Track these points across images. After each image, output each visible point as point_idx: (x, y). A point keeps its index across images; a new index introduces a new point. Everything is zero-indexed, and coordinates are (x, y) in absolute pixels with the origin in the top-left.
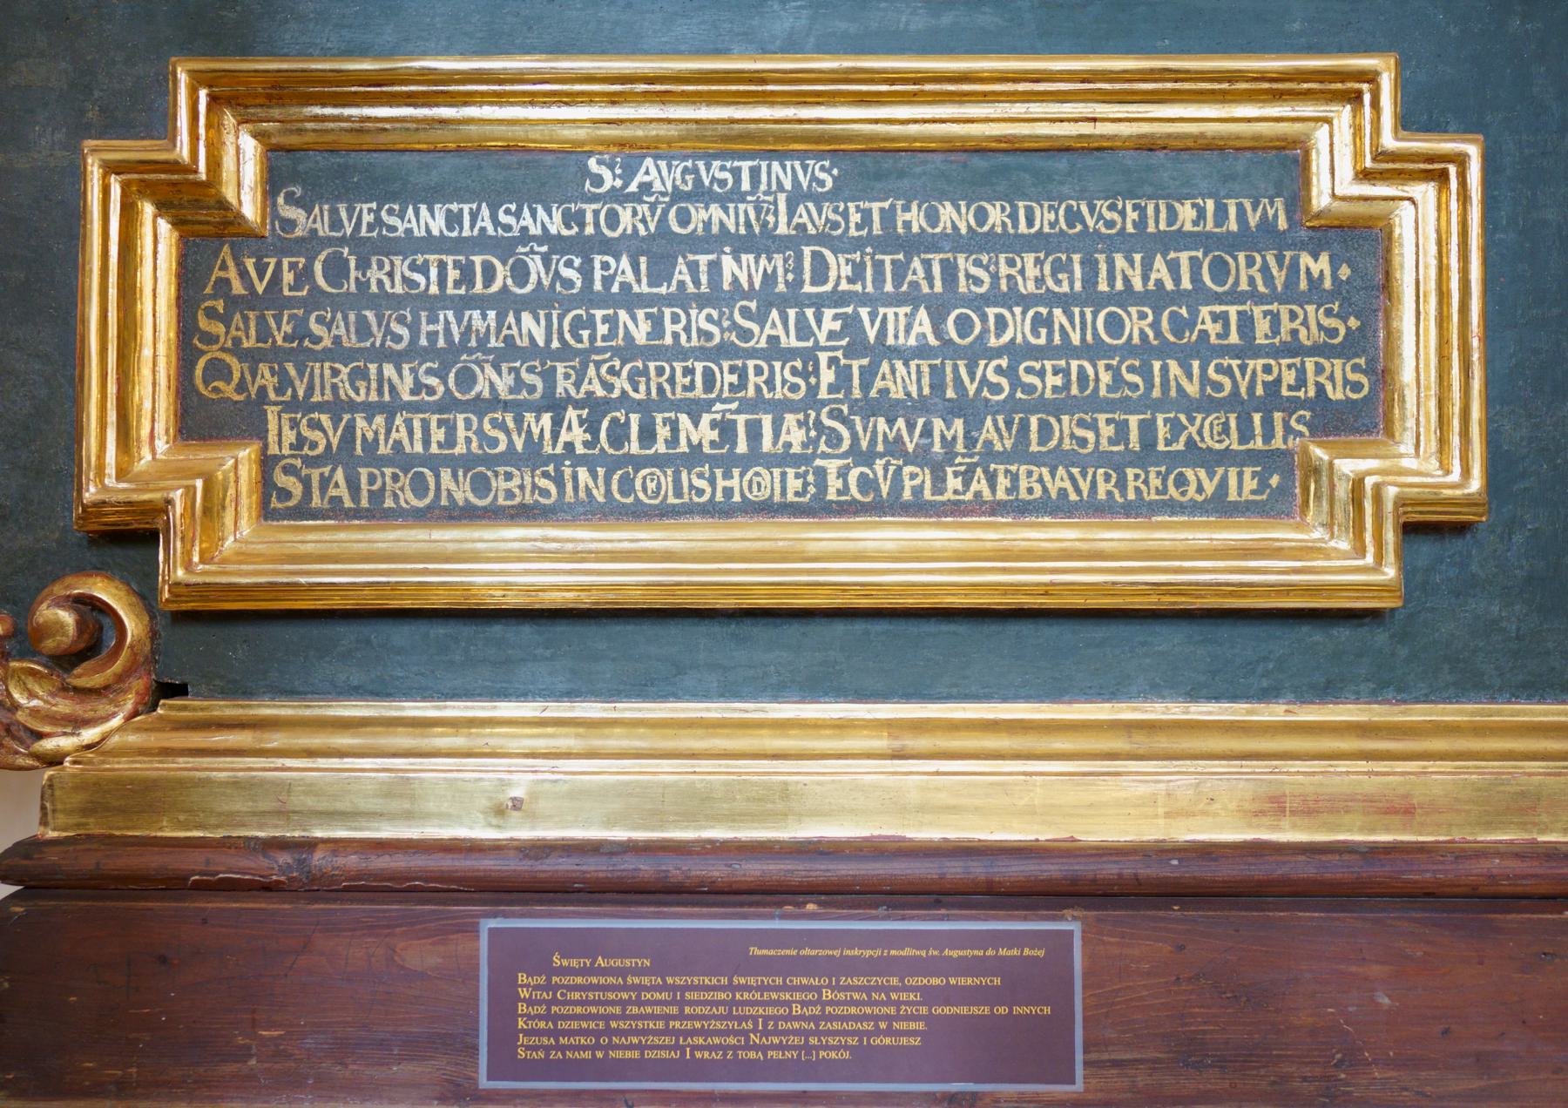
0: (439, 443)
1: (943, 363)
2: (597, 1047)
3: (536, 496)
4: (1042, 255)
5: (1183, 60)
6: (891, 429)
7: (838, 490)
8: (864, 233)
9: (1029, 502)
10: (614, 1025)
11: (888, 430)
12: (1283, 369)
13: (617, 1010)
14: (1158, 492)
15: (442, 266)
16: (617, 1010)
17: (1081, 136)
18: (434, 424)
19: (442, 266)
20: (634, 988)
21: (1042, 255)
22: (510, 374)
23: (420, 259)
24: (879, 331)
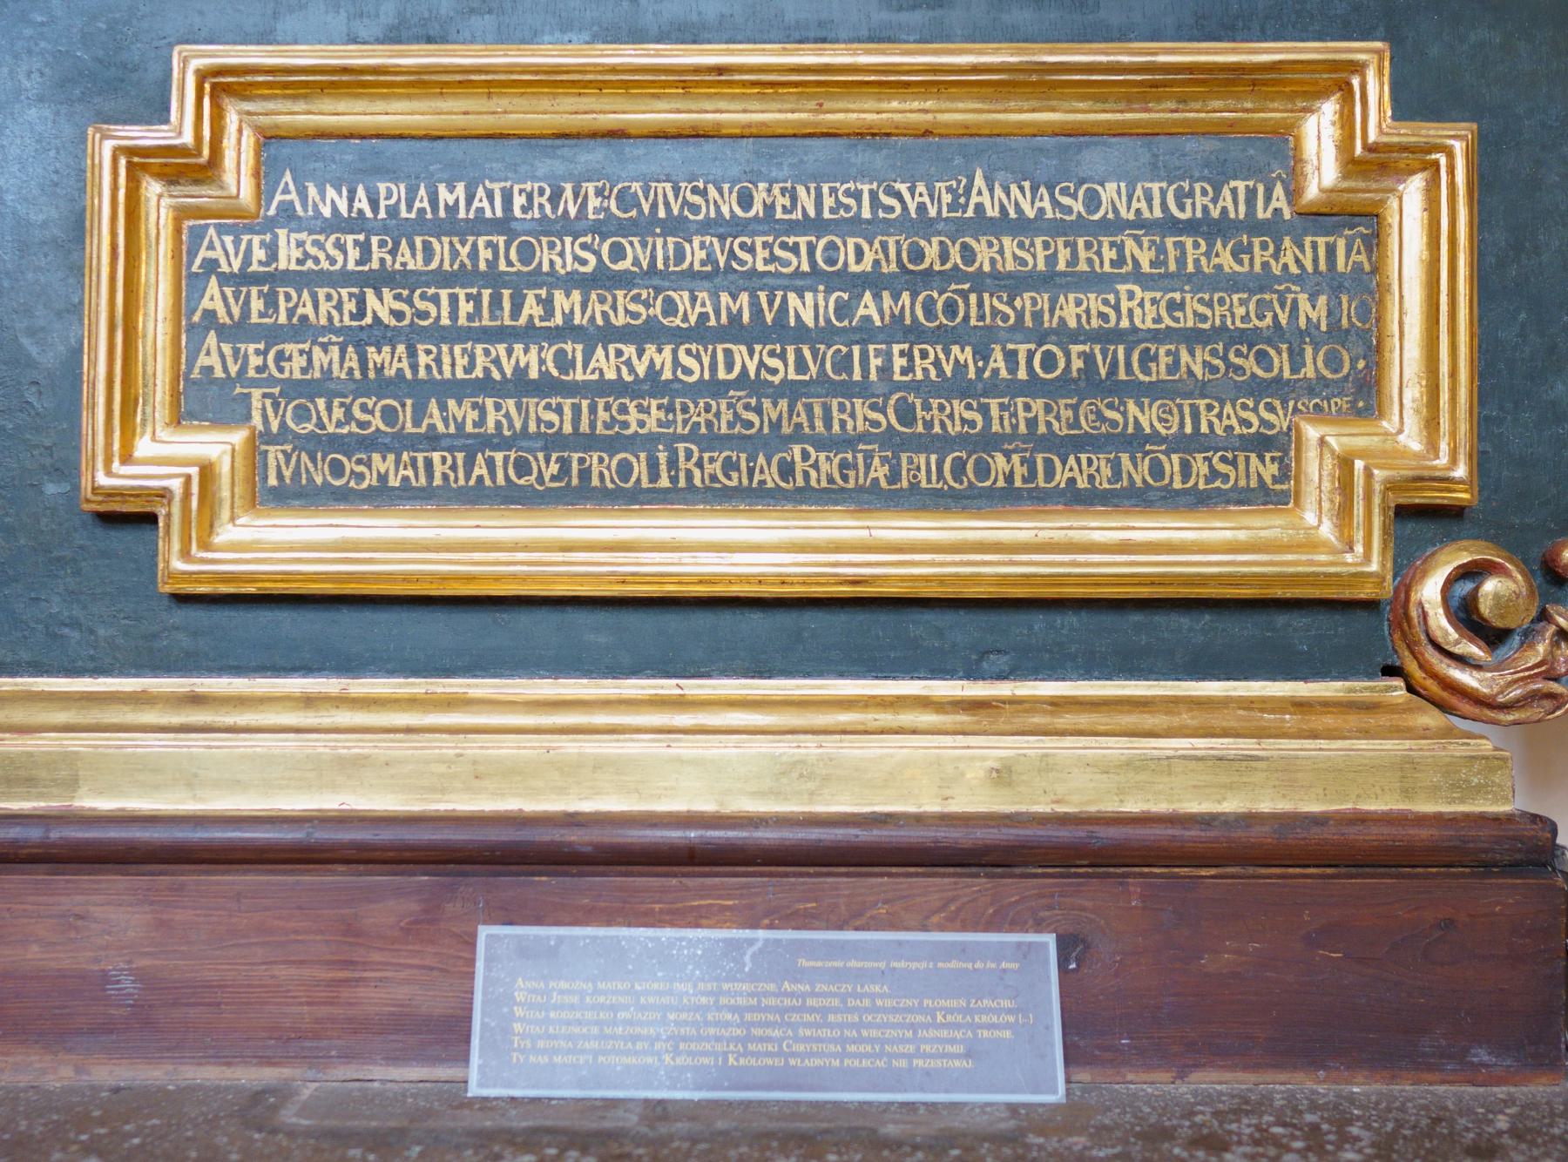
0: (260, 262)
1: (1091, 349)
2: (880, 1056)
3: (628, 319)
4: (832, 455)
5: (1074, 122)
6: (896, 305)
7: (1153, 319)
8: (909, 378)
9: (330, 273)
10: (879, 1003)
11: (731, 304)
12: (1062, 407)
13: (836, 1002)
14: (1070, 427)
15: (454, 299)
16: (836, 1002)
17: (147, 214)
18: (462, 298)
19: (454, 299)
20: (851, 1010)
21: (832, 455)
22: (468, 301)
23: (431, 291)
24: (196, 255)
